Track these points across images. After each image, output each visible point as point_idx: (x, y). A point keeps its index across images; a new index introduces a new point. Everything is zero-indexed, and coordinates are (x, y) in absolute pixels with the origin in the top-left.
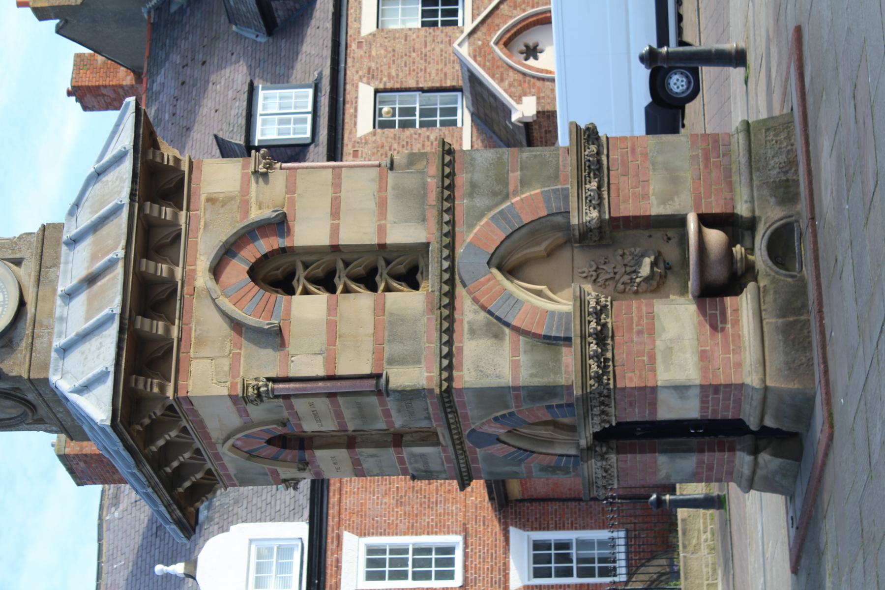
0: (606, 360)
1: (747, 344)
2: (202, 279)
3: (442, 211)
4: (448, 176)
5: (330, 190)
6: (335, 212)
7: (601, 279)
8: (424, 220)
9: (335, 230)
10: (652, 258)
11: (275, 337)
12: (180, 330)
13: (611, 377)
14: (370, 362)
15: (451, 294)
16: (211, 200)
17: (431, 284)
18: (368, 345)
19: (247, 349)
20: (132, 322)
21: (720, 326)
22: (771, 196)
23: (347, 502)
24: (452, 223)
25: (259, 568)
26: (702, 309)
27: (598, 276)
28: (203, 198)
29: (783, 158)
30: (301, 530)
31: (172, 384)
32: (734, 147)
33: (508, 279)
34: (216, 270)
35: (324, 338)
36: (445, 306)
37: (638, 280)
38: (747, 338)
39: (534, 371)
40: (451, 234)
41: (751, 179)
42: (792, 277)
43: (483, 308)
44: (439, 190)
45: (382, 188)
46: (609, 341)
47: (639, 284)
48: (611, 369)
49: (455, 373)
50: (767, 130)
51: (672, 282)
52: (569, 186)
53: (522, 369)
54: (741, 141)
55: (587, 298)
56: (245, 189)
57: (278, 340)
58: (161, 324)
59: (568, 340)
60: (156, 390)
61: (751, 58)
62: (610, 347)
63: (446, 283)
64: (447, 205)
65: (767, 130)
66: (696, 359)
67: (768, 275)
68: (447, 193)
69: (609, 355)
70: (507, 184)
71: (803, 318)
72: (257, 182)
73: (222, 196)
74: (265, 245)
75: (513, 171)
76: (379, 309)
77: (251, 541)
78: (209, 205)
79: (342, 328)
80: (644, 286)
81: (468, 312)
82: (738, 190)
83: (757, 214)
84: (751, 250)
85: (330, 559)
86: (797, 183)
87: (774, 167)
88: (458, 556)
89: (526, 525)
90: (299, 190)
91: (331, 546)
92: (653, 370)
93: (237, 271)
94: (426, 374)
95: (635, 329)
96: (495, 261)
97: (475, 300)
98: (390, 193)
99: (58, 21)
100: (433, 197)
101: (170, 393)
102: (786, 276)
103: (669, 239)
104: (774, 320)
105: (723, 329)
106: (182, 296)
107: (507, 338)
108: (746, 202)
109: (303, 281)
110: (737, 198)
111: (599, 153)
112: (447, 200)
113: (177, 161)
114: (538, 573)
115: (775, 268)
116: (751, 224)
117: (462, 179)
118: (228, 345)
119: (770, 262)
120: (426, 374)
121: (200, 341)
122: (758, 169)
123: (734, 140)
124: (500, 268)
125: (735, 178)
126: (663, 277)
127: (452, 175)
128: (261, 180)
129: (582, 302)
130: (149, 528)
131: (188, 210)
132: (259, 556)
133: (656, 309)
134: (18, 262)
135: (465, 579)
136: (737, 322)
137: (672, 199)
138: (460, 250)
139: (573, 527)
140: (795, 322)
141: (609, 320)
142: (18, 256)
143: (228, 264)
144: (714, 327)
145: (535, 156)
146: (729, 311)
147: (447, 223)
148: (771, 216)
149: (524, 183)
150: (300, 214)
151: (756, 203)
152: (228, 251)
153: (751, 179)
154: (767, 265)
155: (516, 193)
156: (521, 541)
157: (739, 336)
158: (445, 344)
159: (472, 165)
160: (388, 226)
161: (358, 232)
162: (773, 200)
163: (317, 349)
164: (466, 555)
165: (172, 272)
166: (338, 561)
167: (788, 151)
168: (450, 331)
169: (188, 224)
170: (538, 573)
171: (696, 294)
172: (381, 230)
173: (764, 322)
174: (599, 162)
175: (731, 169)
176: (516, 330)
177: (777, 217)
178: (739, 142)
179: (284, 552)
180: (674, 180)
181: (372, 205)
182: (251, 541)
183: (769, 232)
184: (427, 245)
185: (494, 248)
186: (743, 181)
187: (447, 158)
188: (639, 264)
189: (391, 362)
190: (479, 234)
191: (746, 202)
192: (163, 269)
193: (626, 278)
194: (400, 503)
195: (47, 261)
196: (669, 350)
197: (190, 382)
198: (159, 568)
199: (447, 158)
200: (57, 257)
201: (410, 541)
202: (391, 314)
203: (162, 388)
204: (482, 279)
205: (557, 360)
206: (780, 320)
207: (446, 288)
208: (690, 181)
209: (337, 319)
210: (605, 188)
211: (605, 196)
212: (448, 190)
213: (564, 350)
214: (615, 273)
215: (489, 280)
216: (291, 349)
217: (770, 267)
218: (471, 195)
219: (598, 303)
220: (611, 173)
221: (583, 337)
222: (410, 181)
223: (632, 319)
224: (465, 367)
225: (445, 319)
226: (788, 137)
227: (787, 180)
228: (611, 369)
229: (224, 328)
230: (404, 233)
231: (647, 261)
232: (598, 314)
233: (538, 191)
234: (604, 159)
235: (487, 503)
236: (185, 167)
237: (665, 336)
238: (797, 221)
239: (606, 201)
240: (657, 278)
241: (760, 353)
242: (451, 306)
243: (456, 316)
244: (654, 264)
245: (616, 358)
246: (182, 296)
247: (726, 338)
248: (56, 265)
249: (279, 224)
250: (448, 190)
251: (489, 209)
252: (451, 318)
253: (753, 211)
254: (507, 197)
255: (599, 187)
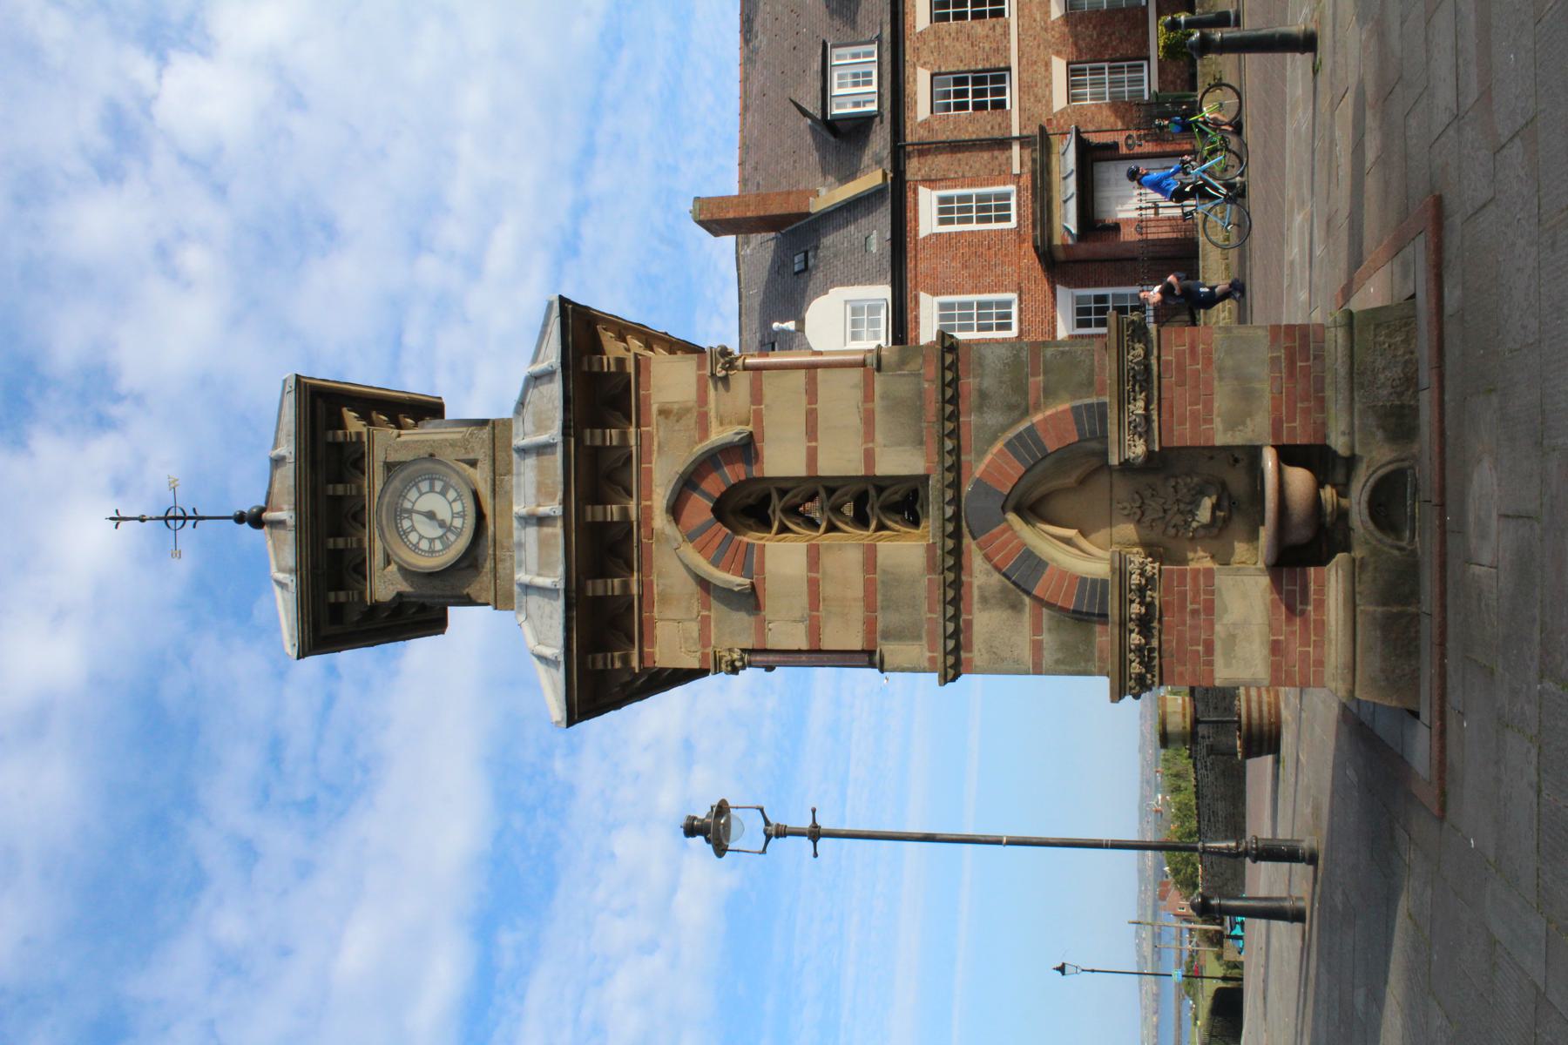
0: (1151, 650)
1: (1333, 636)
2: (660, 521)
3: (943, 437)
4: (949, 385)
5: (804, 399)
6: (812, 431)
7: (1147, 519)
8: (921, 443)
9: (812, 456)
10: (1214, 498)
11: (750, 600)
12: (641, 583)
13: (1157, 673)
14: (861, 635)
15: (957, 552)
16: (664, 412)
17: (931, 525)
18: (857, 613)
19: (717, 610)
20: (581, 588)
21: (1299, 607)
22: (1379, 427)
23: (922, 267)
24: (957, 451)
25: (854, 324)
26: (1276, 583)
27: (1143, 514)
28: (654, 408)
29: (1397, 372)
30: (883, 292)
31: (636, 651)
32: (1329, 345)
33: (1027, 522)
34: (675, 510)
35: (804, 600)
36: (949, 569)
37: (1194, 524)
38: (1333, 629)
39: (1060, 656)
40: (956, 468)
41: (1352, 399)
42: (1401, 549)
43: (997, 568)
44: (939, 405)
45: (868, 396)
46: (1155, 624)
47: (1195, 530)
48: (1156, 662)
49: (963, 655)
50: (1377, 326)
51: (1238, 524)
52: (1107, 399)
53: (1045, 653)
54: (1340, 341)
55: (1130, 567)
56: (702, 399)
57: (752, 601)
58: (617, 581)
59: (1103, 617)
60: (618, 665)
61: (1324, 44)
62: (1156, 633)
63: (950, 536)
64: (949, 426)
65: (1377, 326)
66: (1266, 651)
67: (1367, 542)
68: (949, 408)
69: (1155, 643)
70: (1026, 393)
71: (1412, 609)
72: (716, 389)
73: (676, 407)
74: (733, 473)
75: (1033, 375)
76: (870, 559)
77: (846, 302)
78: (661, 419)
79: (827, 589)
80: (1202, 532)
81: (980, 574)
82: (1333, 411)
83: (1358, 451)
84: (1343, 491)
85: (910, 317)
86: (1415, 410)
87: (1383, 385)
88: (1014, 310)
89: (1071, 283)
90: (767, 399)
91: (910, 305)
92: (1210, 663)
93: (699, 508)
94: (928, 654)
95: (1190, 607)
96: (1011, 503)
97: (988, 558)
98: (878, 404)
99: (345, 410)
100: (932, 408)
101: (635, 663)
102: (1392, 547)
103: (1236, 461)
104: (1371, 608)
105: (1303, 613)
106: (639, 540)
107: (1027, 609)
108: (1343, 433)
109: (779, 514)
110: (1331, 423)
111: (1147, 354)
112: (949, 419)
113: (621, 362)
114: (1080, 324)
115: (1378, 534)
116: (1351, 462)
117: (969, 383)
118: (696, 606)
119: (1371, 526)
120: (928, 654)
121: (665, 599)
122: (1362, 386)
123: (1330, 335)
124: (1018, 511)
125: (1329, 393)
126: (1227, 521)
127: (955, 382)
128: (720, 385)
129: (1122, 573)
130: (772, 266)
131: (638, 426)
132: (853, 314)
133: (1216, 581)
134: (473, 463)
135: (1021, 330)
136: (1320, 604)
137: (1244, 423)
138: (967, 488)
139: (1110, 284)
140: (1400, 615)
141: (1156, 595)
142: (471, 456)
143: (688, 499)
144: (1291, 610)
145: (1063, 353)
146: (1312, 587)
147: (949, 452)
148: (1378, 457)
149: (1049, 393)
150: (769, 433)
151: (1357, 437)
152: (688, 483)
153: (1352, 399)
154: (1365, 529)
155: (1037, 408)
156: (1066, 298)
157: (1323, 622)
158: (950, 619)
159: (981, 365)
160: (877, 450)
161: (840, 459)
162: (1380, 434)
163: (797, 614)
164: (1020, 310)
165: (625, 512)
166: (917, 318)
167: (1406, 362)
168: (956, 601)
169: (639, 446)
170: (1080, 324)
171: (1271, 560)
172: (869, 456)
173: (1358, 610)
174: (1148, 368)
175: (1323, 379)
176: (1039, 601)
177: (1385, 459)
178: (1336, 340)
179: (874, 310)
180: (1246, 394)
181: (855, 421)
182: (846, 302)
183: (1372, 480)
184: (926, 478)
185: (1010, 486)
186: (1341, 402)
187: (949, 359)
188: (1195, 504)
189: (887, 636)
190: (990, 463)
191: (1343, 433)
192: (614, 512)
193: (1178, 519)
194: (965, 267)
195: (500, 468)
196: (1232, 638)
197: (657, 650)
198: (776, 325)
199: (949, 359)
200: (510, 463)
201: (974, 298)
202: (884, 572)
203: (626, 660)
204: (994, 531)
205: (1088, 641)
206: (1380, 609)
207: (950, 544)
208: (1268, 395)
209: (819, 576)
210: (1154, 406)
211: (1155, 417)
212: (951, 395)
213: (1098, 628)
214: (1165, 511)
215: (1004, 531)
216: (768, 612)
217: (1371, 534)
218: (980, 409)
219: (1142, 574)
220: (1164, 381)
221: (1122, 624)
222: (903, 387)
223: (1185, 593)
224: (975, 648)
225: (950, 585)
226: (1406, 341)
227: (1402, 407)
228: (1156, 662)
229: (692, 587)
230: (900, 460)
231: (1207, 503)
232: (1141, 590)
233: (1064, 406)
234: (1154, 362)
235: (1037, 265)
236: (631, 368)
237: (1228, 619)
238: (1412, 467)
239: (1155, 425)
240: (1219, 524)
241: (1349, 656)
242: (958, 567)
243: (964, 578)
244: (1215, 508)
245: (1164, 646)
246: (639, 540)
247: (1305, 623)
248: (509, 472)
249: (746, 449)
250: (951, 395)
251: (1004, 429)
252: (957, 584)
253: (1352, 448)
254: (1026, 413)
255: (1147, 354)
